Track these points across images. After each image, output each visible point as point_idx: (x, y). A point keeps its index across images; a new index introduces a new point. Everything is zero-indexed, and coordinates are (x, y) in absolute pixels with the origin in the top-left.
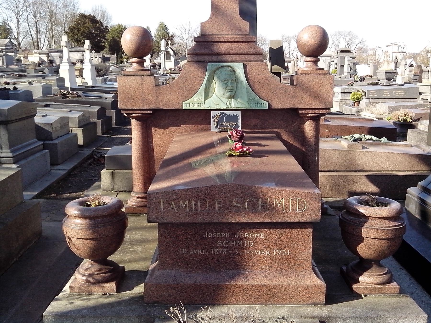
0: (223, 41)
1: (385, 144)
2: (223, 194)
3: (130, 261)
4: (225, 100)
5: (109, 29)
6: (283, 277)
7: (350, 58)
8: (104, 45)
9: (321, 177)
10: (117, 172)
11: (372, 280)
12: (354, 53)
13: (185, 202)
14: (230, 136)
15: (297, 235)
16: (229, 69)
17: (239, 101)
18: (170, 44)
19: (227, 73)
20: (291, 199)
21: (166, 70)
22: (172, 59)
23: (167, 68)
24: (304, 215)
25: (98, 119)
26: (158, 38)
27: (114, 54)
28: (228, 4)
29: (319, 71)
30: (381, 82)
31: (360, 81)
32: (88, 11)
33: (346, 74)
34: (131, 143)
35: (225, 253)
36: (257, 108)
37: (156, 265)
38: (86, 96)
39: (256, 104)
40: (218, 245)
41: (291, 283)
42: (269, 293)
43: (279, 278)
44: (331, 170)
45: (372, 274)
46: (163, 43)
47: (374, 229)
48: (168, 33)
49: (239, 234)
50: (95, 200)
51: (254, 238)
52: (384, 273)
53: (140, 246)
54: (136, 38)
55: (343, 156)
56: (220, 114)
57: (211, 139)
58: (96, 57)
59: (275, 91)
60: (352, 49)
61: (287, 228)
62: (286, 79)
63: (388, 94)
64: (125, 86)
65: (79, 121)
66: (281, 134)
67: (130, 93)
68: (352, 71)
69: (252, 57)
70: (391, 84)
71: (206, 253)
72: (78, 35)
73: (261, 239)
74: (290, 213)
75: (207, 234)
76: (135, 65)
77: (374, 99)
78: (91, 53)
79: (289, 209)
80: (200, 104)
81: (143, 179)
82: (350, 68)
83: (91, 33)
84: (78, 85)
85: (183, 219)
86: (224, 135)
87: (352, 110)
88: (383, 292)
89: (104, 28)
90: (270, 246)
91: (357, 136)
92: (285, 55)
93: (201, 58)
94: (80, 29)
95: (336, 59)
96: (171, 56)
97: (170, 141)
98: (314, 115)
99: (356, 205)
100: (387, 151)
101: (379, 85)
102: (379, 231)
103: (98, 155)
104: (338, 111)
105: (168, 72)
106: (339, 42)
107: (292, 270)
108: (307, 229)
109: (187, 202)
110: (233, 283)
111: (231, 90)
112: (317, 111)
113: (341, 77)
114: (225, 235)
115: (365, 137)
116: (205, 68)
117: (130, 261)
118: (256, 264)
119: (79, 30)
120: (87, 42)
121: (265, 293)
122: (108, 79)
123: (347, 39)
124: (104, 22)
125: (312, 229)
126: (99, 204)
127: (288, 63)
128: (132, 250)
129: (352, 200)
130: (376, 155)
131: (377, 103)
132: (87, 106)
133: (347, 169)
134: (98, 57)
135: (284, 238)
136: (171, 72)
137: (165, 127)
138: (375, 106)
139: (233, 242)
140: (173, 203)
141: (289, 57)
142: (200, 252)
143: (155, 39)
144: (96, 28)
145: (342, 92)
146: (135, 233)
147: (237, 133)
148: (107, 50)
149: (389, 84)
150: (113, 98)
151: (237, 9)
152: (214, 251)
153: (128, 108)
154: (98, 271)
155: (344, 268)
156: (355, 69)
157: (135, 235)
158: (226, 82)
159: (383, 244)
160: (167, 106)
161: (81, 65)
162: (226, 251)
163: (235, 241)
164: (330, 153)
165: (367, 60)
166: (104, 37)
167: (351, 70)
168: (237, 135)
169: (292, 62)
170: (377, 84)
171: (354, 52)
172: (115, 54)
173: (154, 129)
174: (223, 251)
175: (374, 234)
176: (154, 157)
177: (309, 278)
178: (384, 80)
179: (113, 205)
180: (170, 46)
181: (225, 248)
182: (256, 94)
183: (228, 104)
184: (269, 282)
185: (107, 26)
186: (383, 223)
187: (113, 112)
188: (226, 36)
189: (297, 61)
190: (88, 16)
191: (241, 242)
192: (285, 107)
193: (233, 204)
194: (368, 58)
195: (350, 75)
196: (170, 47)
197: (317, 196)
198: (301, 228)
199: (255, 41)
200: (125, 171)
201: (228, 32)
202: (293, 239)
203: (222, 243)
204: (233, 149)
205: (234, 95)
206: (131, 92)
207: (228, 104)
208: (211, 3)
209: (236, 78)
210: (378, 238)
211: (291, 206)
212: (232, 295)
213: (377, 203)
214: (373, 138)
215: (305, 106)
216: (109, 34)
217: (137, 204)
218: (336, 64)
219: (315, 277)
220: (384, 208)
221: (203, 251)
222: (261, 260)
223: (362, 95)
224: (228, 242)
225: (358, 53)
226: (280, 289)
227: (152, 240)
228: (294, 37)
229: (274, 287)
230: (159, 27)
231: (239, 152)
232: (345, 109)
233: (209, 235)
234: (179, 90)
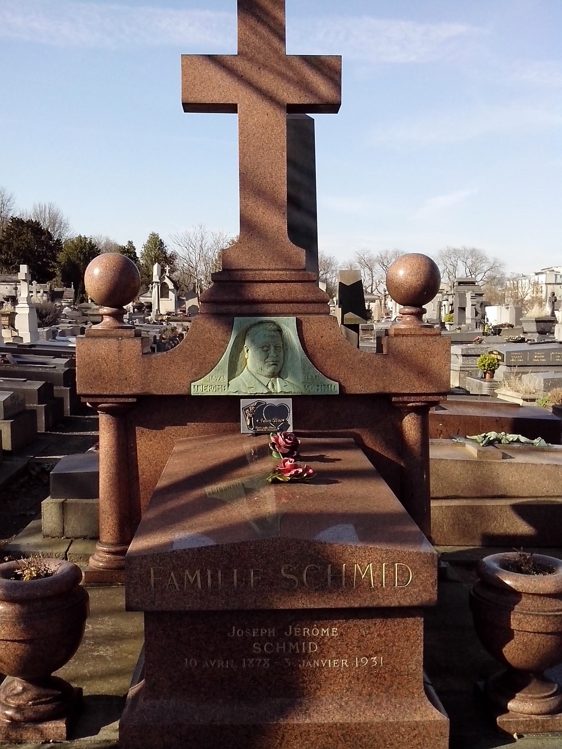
0: (261, 279)
1: (541, 450)
2: (262, 558)
3: (92, 677)
4: (265, 380)
5: (62, 245)
6: (372, 709)
7: (476, 294)
8: (54, 271)
9: (434, 508)
10: (72, 504)
11: (530, 708)
12: (480, 285)
13: (195, 572)
14: (273, 444)
15: (396, 630)
16: (272, 327)
17: (288, 382)
18: (167, 271)
19: (267, 333)
20: (384, 564)
21: (161, 314)
22: (172, 295)
23: (163, 312)
24: (408, 594)
25: (39, 404)
26: (147, 261)
27: (70, 287)
28: (270, 219)
29: (424, 331)
30: (530, 337)
31: (492, 334)
32: (27, 213)
33: (468, 321)
34: (98, 448)
35: (266, 665)
36: (320, 393)
37: (139, 687)
38: (19, 362)
39: (318, 386)
40: (254, 652)
41: (387, 719)
42: (348, 738)
43: (365, 710)
44: (449, 496)
45: (530, 696)
46: (156, 268)
47: (531, 614)
48: (165, 253)
49: (293, 630)
50: (31, 567)
51: (320, 637)
52: (551, 692)
53: (111, 646)
54: (111, 273)
55: (470, 472)
56: (256, 403)
57: (240, 448)
58: (39, 292)
59: (352, 364)
60: (479, 278)
61: (377, 617)
62: (368, 332)
63: (542, 358)
64: (89, 355)
65: (6, 408)
66: (363, 438)
67: (98, 367)
68: (479, 316)
69: (311, 307)
70: (546, 340)
71: (232, 666)
72: (8, 254)
73: (332, 638)
74: (384, 590)
75: (234, 630)
76: (107, 319)
77: (518, 366)
78: (30, 285)
79: (381, 583)
80: (220, 386)
81: (118, 519)
82: (476, 312)
83: (32, 251)
84: (5, 343)
85: (190, 605)
86: (262, 441)
87: (481, 385)
88: (550, 728)
89: (54, 242)
90: (349, 650)
91: (492, 435)
92: (364, 288)
93: (223, 309)
94: (13, 244)
95: (451, 297)
96: (170, 291)
97: (167, 450)
98: (419, 404)
99: (497, 571)
100: (545, 462)
101: (527, 342)
102: (541, 619)
103: (37, 469)
104: (458, 386)
105: (164, 319)
106: (455, 267)
107: (388, 694)
108: (413, 619)
109: (198, 572)
110: (282, 722)
111: (275, 363)
112: (423, 398)
113: (460, 329)
114: (268, 632)
115: (507, 437)
116: (230, 326)
117: (92, 677)
118: (323, 685)
119: (10, 245)
120: (24, 268)
121: (340, 739)
122: (59, 331)
123: (469, 262)
124: (54, 233)
125: (423, 619)
126: (36, 574)
127: (370, 303)
128: (96, 654)
129: (491, 560)
130: (527, 469)
131: (523, 373)
132: (21, 381)
133: (479, 495)
134: (42, 291)
135: (373, 635)
136: (169, 318)
137: (158, 426)
138: (520, 379)
139: (281, 645)
140: (172, 574)
141: (372, 292)
142: (221, 664)
143: (142, 262)
144: (41, 243)
145: (463, 354)
146: (103, 621)
147: (286, 439)
148: (58, 279)
149: (543, 341)
150: (66, 365)
151: (285, 227)
152: (247, 663)
153: (93, 393)
154: (34, 699)
155: (481, 684)
156: (483, 313)
157: (102, 625)
158: (265, 348)
159: (548, 642)
160: (163, 390)
161: (12, 307)
162: (269, 662)
163: (284, 644)
164: (447, 466)
165: (503, 297)
166: (54, 258)
167: (477, 314)
168: (286, 443)
169: (377, 302)
170: (522, 341)
171: (480, 283)
172: (72, 287)
173: (139, 430)
174: (264, 662)
175: (532, 624)
176: (138, 478)
177: (419, 707)
178: (534, 334)
179: (63, 576)
180: (167, 274)
181: (267, 656)
182: (317, 369)
183: (270, 386)
184: (347, 719)
185: (60, 240)
186: (547, 604)
187: (66, 390)
188: (266, 272)
189: (386, 300)
190: (27, 222)
191: (297, 644)
192: (368, 392)
193: (281, 575)
194: (504, 294)
195: (476, 323)
196: (168, 277)
197: (430, 560)
198: (403, 617)
199: (315, 281)
200: (85, 501)
201: (269, 265)
202: (390, 637)
203: (262, 648)
204: (279, 469)
205: (280, 372)
206: (100, 365)
207: (270, 386)
208: (241, 216)
209: (283, 341)
210: (540, 631)
211: (385, 577)
212: (281, 744)
213: (535, 567)
214: (520, 438)
215: (402, 389)
216: (62, 253)
217: (105, 564)
218: (452, 305)
219: (430, 707)
220: (549, 576)
221: (227, 663)
222: (332, 678)
223: (497, 359)
224: (272, 645)
225: (488, 286)
226: (367, 731)
227: (132, 635)
228: (380, 259)
229: (356, 728)
230: (149, 242)
231: (291, 475)
232: (469, 384)
233: (238, 633)
234: (184, 363)
